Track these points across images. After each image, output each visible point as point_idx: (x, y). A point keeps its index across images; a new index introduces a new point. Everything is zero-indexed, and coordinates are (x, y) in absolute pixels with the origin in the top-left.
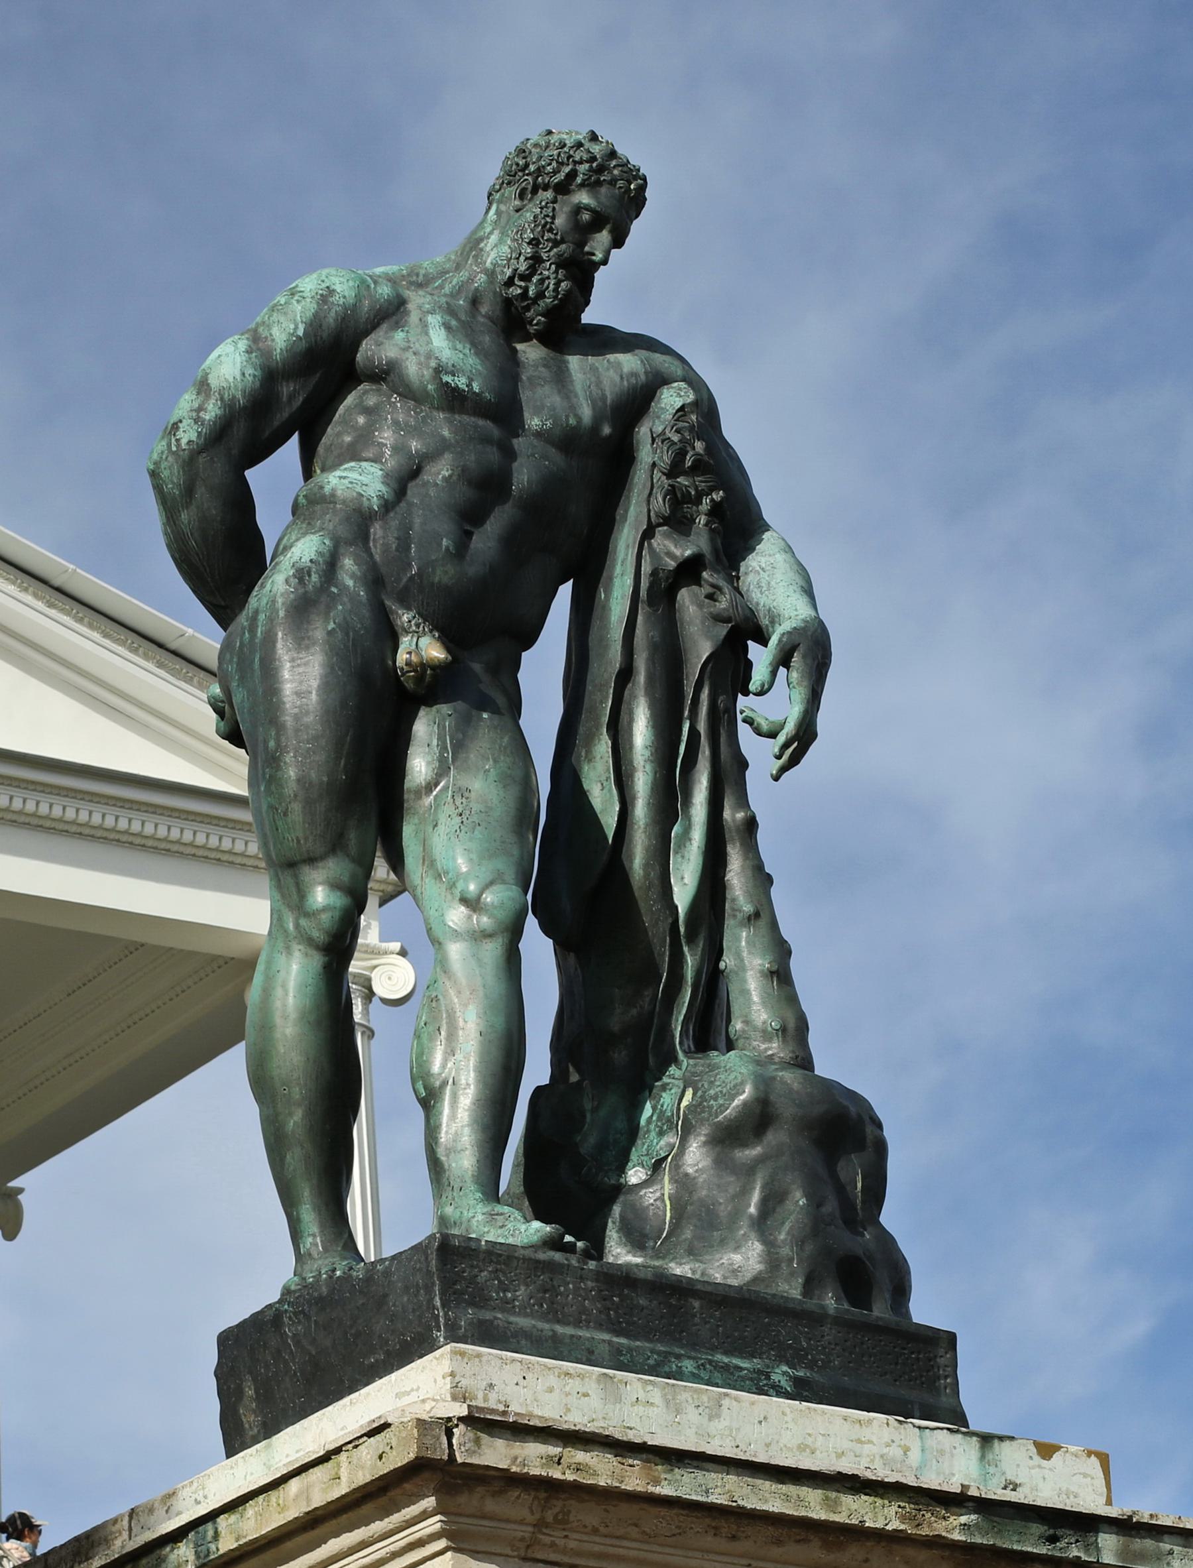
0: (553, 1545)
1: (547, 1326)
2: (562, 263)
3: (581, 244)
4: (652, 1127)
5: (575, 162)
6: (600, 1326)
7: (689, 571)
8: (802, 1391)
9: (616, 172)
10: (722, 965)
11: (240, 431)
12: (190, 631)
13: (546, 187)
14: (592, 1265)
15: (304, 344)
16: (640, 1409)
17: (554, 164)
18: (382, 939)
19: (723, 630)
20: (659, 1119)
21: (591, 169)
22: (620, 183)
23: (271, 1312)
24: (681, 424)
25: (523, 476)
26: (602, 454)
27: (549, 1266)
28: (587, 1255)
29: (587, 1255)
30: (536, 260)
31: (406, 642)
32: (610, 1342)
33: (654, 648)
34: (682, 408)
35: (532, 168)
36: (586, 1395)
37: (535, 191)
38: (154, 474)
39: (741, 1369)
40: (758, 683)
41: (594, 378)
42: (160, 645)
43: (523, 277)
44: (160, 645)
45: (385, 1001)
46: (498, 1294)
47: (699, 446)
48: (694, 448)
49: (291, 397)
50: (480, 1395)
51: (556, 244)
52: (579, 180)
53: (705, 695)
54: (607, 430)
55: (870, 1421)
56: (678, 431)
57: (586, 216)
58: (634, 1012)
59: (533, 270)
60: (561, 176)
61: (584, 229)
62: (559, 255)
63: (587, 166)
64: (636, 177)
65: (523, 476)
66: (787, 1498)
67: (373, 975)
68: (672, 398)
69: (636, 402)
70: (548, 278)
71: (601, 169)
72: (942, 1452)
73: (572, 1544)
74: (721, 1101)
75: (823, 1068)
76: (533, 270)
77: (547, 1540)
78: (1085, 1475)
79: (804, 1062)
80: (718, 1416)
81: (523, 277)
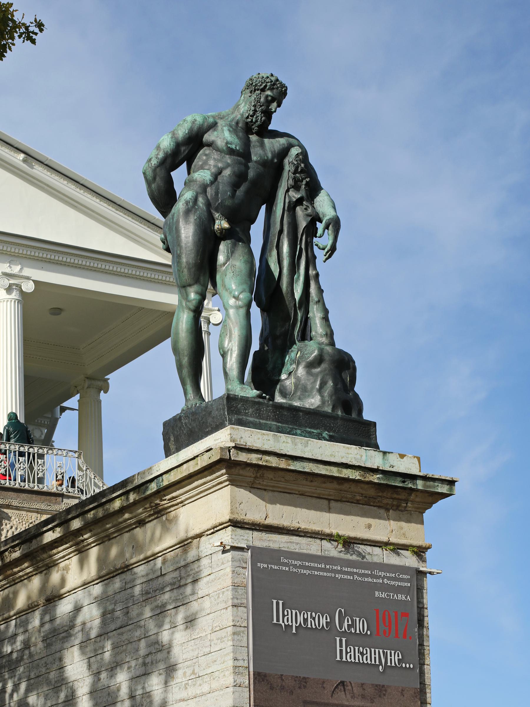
0: (259, 483)
2: (262, 112)
6: (273, 420)
7: (299, 202)
8: (331, 439)
10: (309, 316)
11: (169, 161)
13: (258, 90)
14: (271, 402)
15: (188, 136)
16: (284, 444)
22: (279, 89)
27: (259, 403)
28: (269, 400)
32: (276, 425)
34: (297, 154)
35: (254, 84)
36: (269, 440)
37: (255, 91)
38: (144, 174)
39: (314, 433)
42: (149, 221)
43: (251, 116)
44: (149, 221)
45: (213, 324)
47: (303, 165)
49: (184, 151)
50: (239, 440)
51: (261, 106)
52: (268, 88)
54: (276, 161)
55: (351, 448)
57: (270, 98)
61: (268, 102)
62: (262, 110)
64: (284, 87)
66: (327, 470)
68: (295, 151)
69: (284, 152)
71: (274, 84)
72: (372, 457)
73: (265, 483)
75: (338, 346)
77: (258, 482)
78: (413, 463)
79: (332, 343)
80: (307, 446)
81: (251, 116)
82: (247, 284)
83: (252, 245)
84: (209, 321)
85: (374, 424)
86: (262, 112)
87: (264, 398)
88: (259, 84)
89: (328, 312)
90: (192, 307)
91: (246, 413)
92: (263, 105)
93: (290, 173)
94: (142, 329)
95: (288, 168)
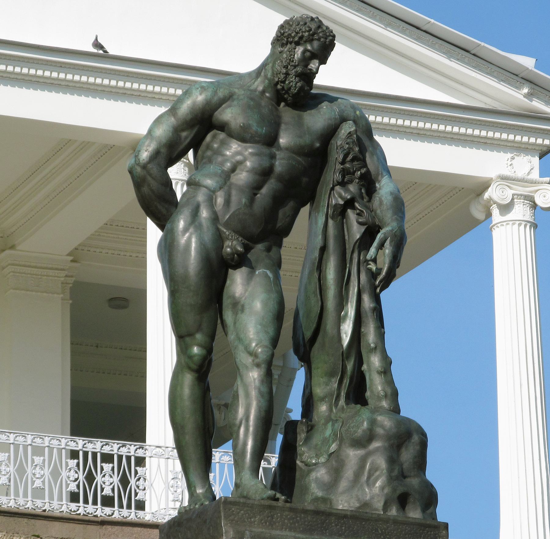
1: (268, 531)
2: (298, 75)
3: (306, 66)
4: (331, 438)
5: (302, 32)
7: (350, 204)
9: (321, 35)
10: (363, 369)
12: (432, 21)
13: (291, 43)
14: (288, 505)
17: (294, 33)
18: (541, 176)
19: (363, 229)
20: (334, 435)
21: (309, 35)
22: (322, 40)
23: (172, 523)
24: (348, 140)
25: (279, 166)
26: (316, 155)
27: (270, 507)
28: (286, 501)
29: (286, 501)
30: (287, 74)
31: (228, 243)
33: (336, 237)
34: (350, 133)
35: (286, 34)
37: (287, 44)
38: (131, 172)
40: (370, 256)
41: (318, 119)
42: (418, 28)
43: (282, 82)
44: (418, 28)
45: (542, 209)
46: (248, 519)
47: (357, 149)
48: (353, 151)
51: (295, 67)
52: (304, 39)
53: (356, 255)
54: (318, 145)
56: (347, 144)
57: (308, 54)
58: (328, 387)
59: (286, 78)
60: (296, 39)
61: (306, 60)
62: (296, 72)
63: (307, 34)
64: (330, 36)
65: (279, 166)
67: (535, 196)
68: (348, 128)
69: (330, 133)
70: (292, 81)
71: (313, 35)
74: (354, 429)
75: (404, 413)
76: (286, 78)
79: (396, 410)
81: (282, 82)
82: (266, 332)
83: (281, 273)
84: (534, 202)
85: (446, 526)
86: (298, 75)
87: (277, 500)
88: (293, 35)
89: (391, 363)
90: (195, 367)
91: (251, 522)
92: (298, 65)
93: (338, 163)
94: (421, 216)
95: (336, 155)
